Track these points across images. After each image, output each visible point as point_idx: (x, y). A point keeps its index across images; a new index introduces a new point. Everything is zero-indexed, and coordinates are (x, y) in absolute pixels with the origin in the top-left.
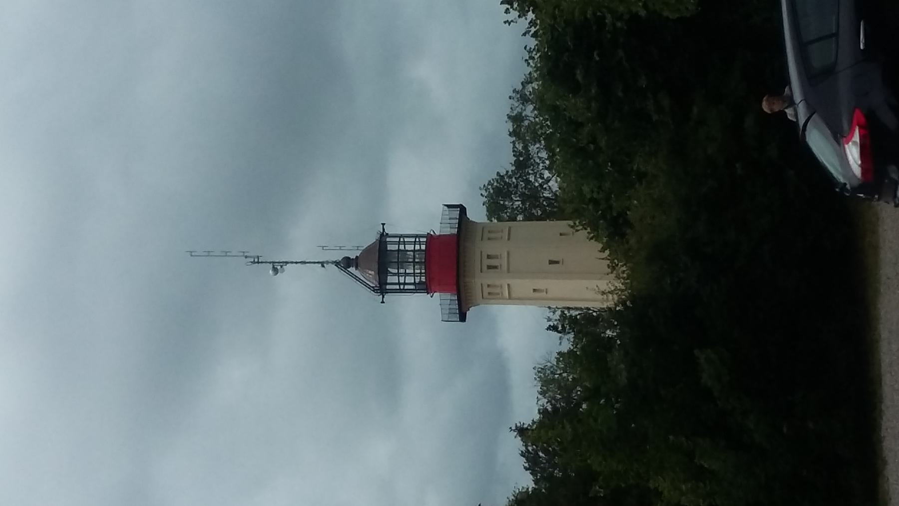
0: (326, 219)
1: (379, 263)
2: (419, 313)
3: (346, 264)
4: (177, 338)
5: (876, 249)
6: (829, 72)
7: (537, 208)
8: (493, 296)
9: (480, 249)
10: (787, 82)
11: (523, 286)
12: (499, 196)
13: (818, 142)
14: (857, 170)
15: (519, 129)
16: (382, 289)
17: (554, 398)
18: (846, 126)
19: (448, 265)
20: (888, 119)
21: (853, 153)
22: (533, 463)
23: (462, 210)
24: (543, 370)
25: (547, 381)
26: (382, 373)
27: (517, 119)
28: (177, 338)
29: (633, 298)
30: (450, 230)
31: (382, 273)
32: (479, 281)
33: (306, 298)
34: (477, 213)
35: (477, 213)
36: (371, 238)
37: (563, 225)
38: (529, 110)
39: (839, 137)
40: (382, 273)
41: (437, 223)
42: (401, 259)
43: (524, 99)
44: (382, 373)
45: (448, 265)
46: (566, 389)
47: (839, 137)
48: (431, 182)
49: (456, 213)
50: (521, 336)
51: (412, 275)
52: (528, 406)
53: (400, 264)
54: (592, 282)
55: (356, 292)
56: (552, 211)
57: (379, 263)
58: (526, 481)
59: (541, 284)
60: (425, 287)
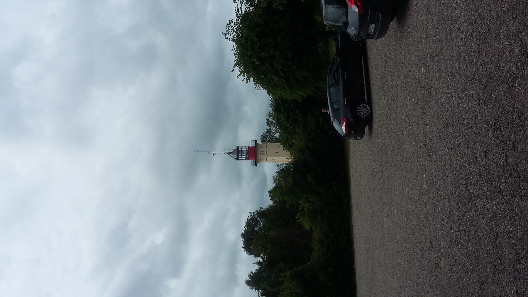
0: (224, 143)
1: (237, 153)
2: (246, 165)
3: (230, 153)
4: (190, 169)
5: (349, 149)
6: (338, 109)
7: (274, 141)
8: (263, 160)
9: (260, 150)
10: (339, 84)
11: (270, 158)
12: (264, 138)
13: (336, 125)
14: (345, 132)
15: (269, 122)
16: (238, 159)
17: (277, 201)
18: (342, 121)
19: (253, 153)
20: (352, 120)
21: (344, 128)
22: (272, 198)
23: (256, 141)
24: (274, 177)
25: (275, 180)
26: (238, 177)
27: (268, 120)
28: (190, 169)
29: (295, 162)
30: (253, 145)
31: (238, 155)
32: (260, 157)
33: (220, 161)
34: (259, 142)
35: (259, 142)
36: (236, 147)
37: (279, 144)
38: (271, 119)
39: (340, 124)
40: (238, 155)
41: (250, 144)
42: (242, 152)
43: (270, 116)
44: (238, 177)
45: (253, 153)
46: (280, 182)
47: (340, 124)
48: (248, 135)
49: (254, 142)
50: (270, 167)
51: (245, 156)
52: (271, 185)
53: (242, 153)
54: (285, 158)
55: (232, 160)
56: (277, 141)
57: (237, 153)
58: (271, 202)
59: (274, 158)
60: (247, 159)
